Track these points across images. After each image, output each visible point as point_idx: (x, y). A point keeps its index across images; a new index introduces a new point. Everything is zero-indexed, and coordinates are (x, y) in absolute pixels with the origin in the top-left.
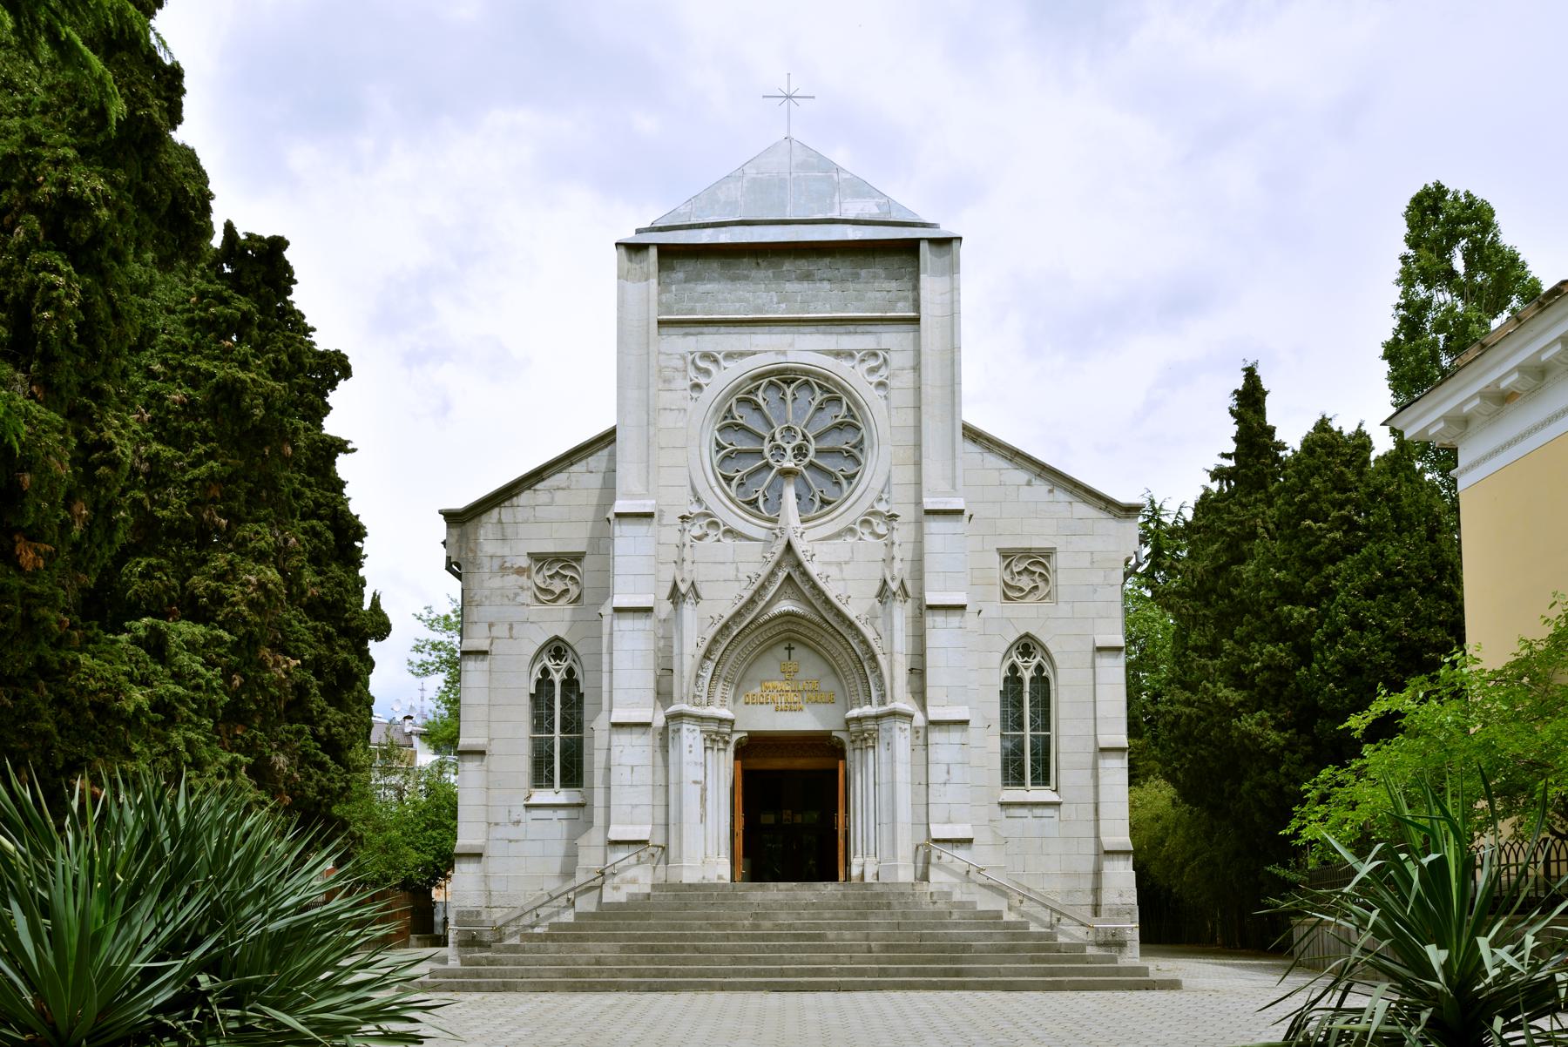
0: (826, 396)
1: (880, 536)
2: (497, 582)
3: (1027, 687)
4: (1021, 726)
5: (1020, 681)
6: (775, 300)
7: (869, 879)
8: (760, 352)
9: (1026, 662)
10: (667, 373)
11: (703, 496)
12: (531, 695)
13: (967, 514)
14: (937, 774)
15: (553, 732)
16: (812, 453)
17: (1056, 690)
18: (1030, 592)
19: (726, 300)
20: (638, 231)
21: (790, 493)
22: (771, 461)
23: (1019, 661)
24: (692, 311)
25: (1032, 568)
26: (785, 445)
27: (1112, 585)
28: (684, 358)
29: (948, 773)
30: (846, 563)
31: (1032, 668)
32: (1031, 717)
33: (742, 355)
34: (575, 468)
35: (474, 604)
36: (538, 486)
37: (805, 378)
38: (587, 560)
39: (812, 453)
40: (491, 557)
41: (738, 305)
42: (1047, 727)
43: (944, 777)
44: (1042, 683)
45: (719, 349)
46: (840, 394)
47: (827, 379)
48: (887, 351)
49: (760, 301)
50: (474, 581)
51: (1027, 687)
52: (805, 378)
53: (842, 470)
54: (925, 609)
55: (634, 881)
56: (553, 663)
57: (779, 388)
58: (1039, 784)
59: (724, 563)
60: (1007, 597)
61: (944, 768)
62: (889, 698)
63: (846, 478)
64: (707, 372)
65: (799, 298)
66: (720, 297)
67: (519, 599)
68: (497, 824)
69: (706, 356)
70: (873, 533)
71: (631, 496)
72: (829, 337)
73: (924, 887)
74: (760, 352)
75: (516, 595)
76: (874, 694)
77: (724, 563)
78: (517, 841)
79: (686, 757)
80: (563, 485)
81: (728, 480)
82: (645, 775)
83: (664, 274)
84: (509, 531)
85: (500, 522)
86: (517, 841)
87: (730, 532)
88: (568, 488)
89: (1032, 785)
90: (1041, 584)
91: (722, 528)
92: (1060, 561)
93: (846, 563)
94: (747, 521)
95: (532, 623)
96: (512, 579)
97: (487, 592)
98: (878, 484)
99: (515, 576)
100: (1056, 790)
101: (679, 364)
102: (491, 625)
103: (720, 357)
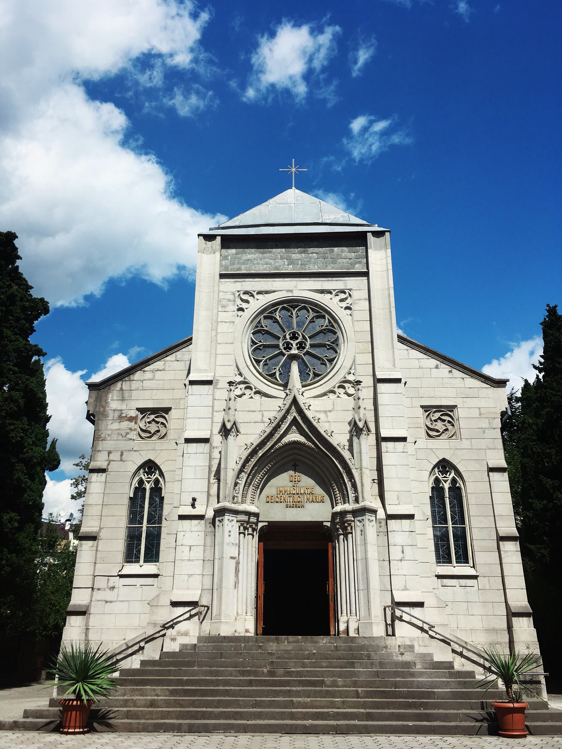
0: (316, 314)
1: (349, 395)
2: (116, 426)
3: (447, 494)
4: (446, 522)
5: (443, 489)
6: (286, 263)
7: (352, 634)
8: (277, 291)
9: (445, 477)
10: (224, 302)
11: (243, 371)
12: (130, 498)
13: (403, 381)
14: (395, 553)
15: (142, 524)
16: (308, 346)
17: (466, 496)
18: (443, 432)
19: (258, 264)
20: (211, 229)
21: (295, 368)
22: (284, 351)
23: (440, 477)
24: (240, 269)
25: (443, 417)
26: (292, 342)
27: (494, 429)
28: (234, 294)
29: (403, 552)
30: (330, 411)
31: (449, 481)
32: (451, 515)
33: (267, 292)
34: (168, 358)
35: (101, 439)
36: (146, 369)
37: (303, 305)
38: (173, 413)
39: (308, 346)
40: (114, 410)
41: (265, 266)
42: (463, 522)
43: (400, 556)
44: (456, 492)
45: (254, 289)
46: (324, 313)
47: (316, 305)
48: (350, 290)
49: (278, 264)
50: (103, 425)
51: (447, 494)
52: (303, 305)
53: (326, 356)
54: (380, 440)
55: (186, 634)
56: (146, 477)
57: (288, 310)
58: (461, 563)
59: (254, 411)
60: (429, 435)
61: (400, 548)
62: (360, 499)
63: (329, 360)
64: (247, 302)
65: (300, 263)
66: (255, 262)
67: (129, 436)
68: (99, 589)
69: (246, 293)
70: (346, 393)
71: (199, 371)
72: (317, 283)
73: (390, 641)
74: (277, 291)
75: (127, 433)
76: (352, 495)
77: (254, 411)
78: (111, 602)
79: (227, 539)
80: (161, 369)
81: (258, 362)
82: (198, 553)
83: (224, 251)
84: (126, 395)
85: (121, 389)
86: (111, 602)
87: (258, 392)
88: (164, 370)
89: (457, 563)
90: (450, 427)
91: (254, 390)
92: (460, 413)
93: (330, 411)
94: (269, 386)
95: (135, 451)
96: (125, 425)
97: (109, 432)
98: (348, 364)
99: (128, 422)
100: (474, 567)
101: (231, 297)
102: (109, 453)
103: (255, 294)
